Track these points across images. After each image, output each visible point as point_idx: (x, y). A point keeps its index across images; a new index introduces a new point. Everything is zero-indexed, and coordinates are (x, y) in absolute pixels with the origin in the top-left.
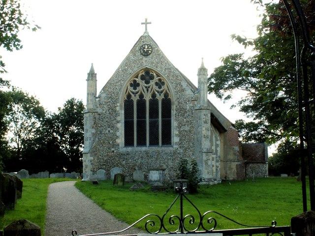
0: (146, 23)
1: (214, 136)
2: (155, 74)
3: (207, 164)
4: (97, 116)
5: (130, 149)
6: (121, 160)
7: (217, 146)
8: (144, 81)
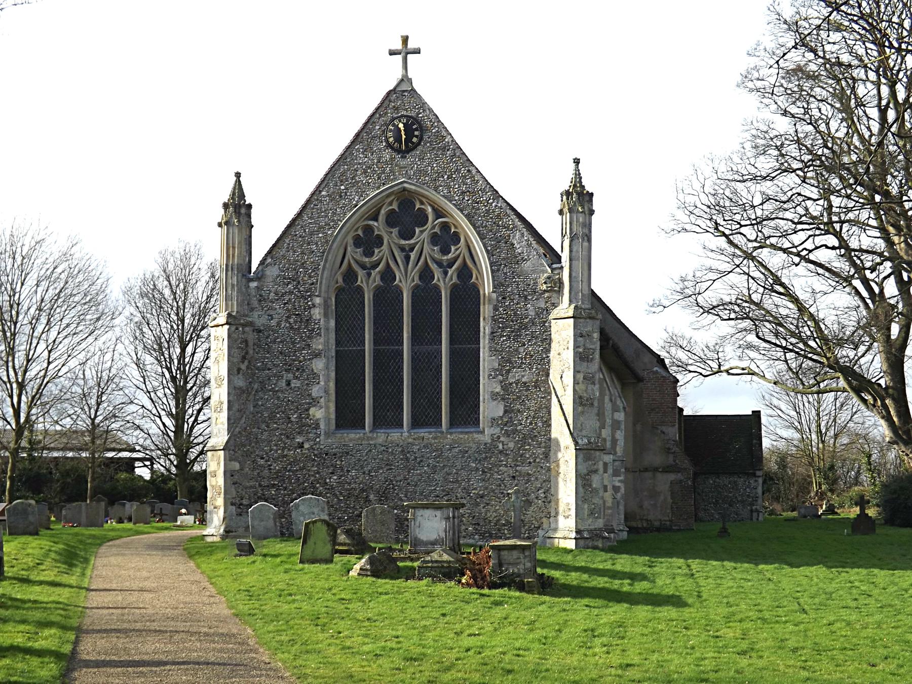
0: (405, 51)
1: (607, 399)
2: (430, 209)
3: (590, 486)
4: (252, 337)
5: (352, 436)
6: (325, 472)
7: (616, 425)
8: (395, 231)
